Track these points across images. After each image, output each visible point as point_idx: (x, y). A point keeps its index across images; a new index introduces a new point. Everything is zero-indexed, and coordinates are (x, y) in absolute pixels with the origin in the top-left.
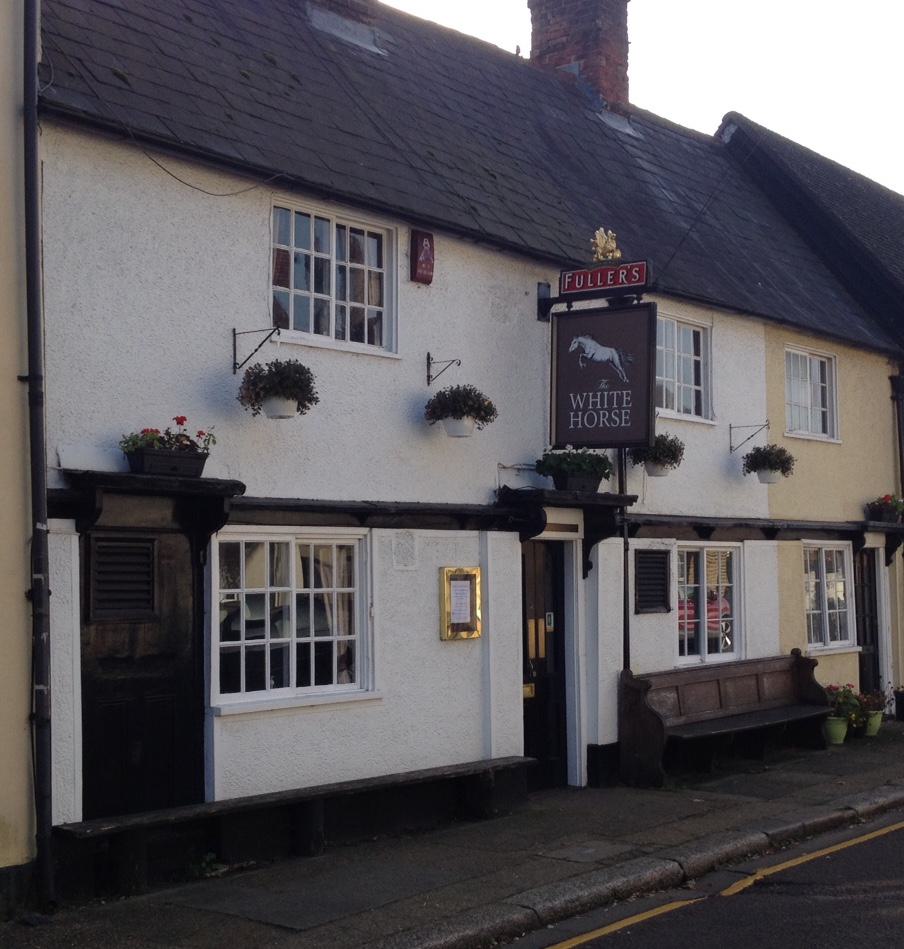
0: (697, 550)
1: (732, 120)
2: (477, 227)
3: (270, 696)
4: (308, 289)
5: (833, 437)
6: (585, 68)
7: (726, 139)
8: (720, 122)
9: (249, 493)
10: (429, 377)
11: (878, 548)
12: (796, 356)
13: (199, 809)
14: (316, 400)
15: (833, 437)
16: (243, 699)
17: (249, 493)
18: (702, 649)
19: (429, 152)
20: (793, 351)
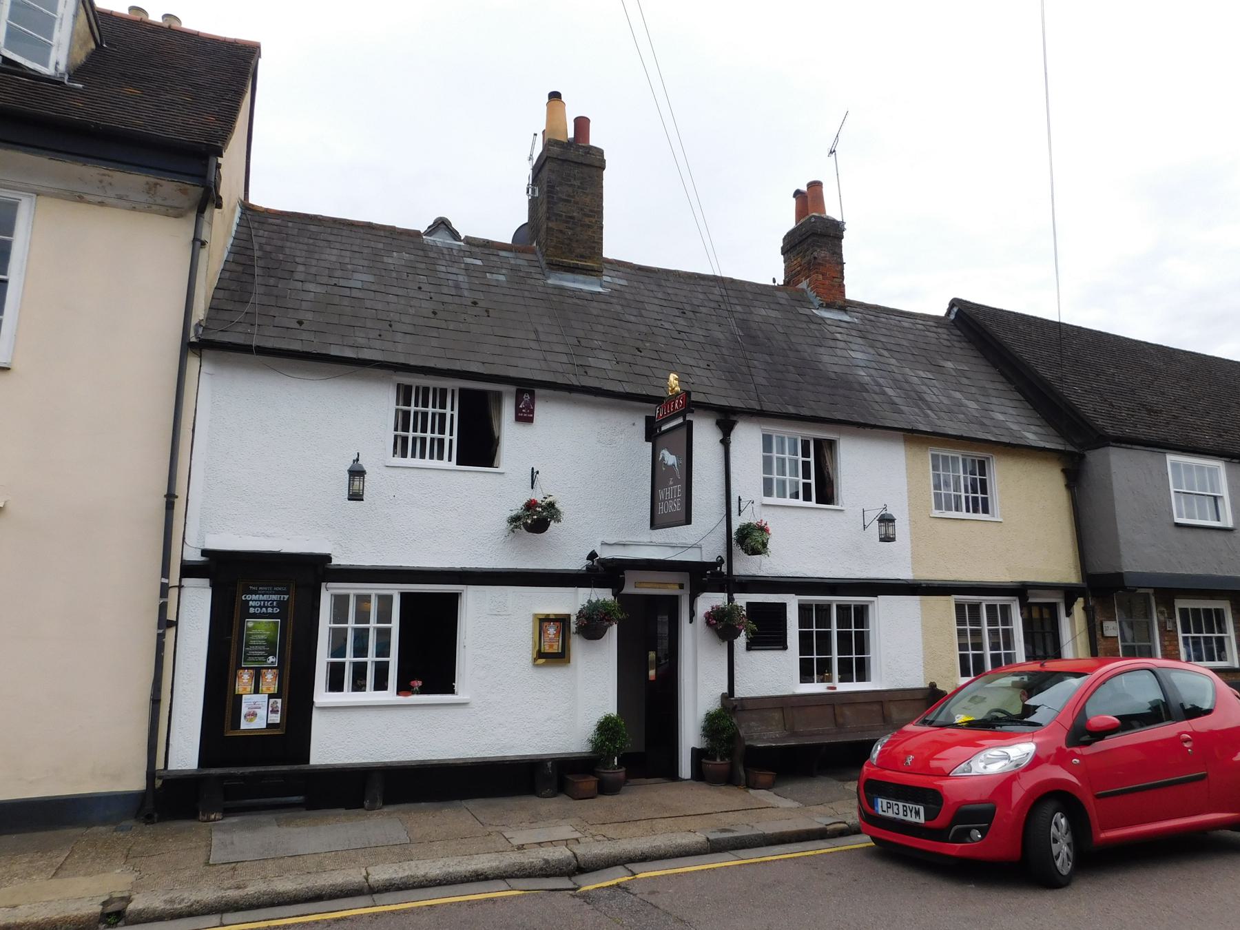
0: (829, 603)
1: (955, 303)
2: (571, 383)
3: (370, 696)
4: (797, 476)
5: (994, 516)
6: (810, 283)
7: (952, 317)
8: (948, 306)
9: (335, 562)
10: (740, 510)
11: (1059, 603)
12: (945, 458)
13: (303, 767)
14: (559, 521)
15: (994, 516)
16: (347, 696)
17: (335, 562)
18: (834, 680)
19: (641, 352)
20: (950, 455)
